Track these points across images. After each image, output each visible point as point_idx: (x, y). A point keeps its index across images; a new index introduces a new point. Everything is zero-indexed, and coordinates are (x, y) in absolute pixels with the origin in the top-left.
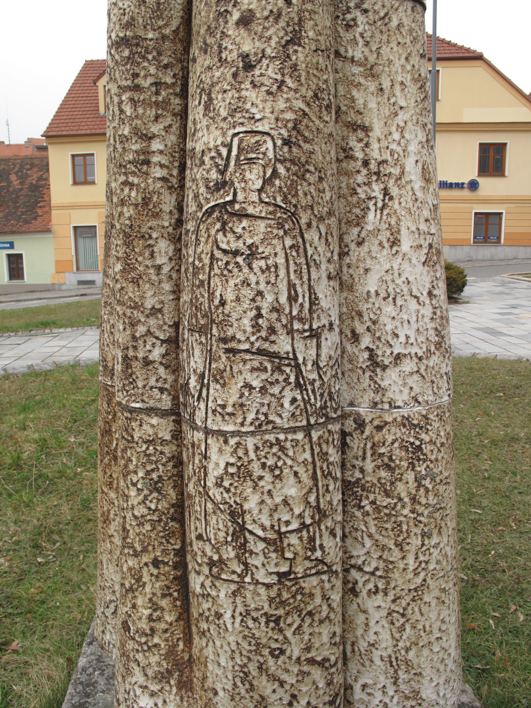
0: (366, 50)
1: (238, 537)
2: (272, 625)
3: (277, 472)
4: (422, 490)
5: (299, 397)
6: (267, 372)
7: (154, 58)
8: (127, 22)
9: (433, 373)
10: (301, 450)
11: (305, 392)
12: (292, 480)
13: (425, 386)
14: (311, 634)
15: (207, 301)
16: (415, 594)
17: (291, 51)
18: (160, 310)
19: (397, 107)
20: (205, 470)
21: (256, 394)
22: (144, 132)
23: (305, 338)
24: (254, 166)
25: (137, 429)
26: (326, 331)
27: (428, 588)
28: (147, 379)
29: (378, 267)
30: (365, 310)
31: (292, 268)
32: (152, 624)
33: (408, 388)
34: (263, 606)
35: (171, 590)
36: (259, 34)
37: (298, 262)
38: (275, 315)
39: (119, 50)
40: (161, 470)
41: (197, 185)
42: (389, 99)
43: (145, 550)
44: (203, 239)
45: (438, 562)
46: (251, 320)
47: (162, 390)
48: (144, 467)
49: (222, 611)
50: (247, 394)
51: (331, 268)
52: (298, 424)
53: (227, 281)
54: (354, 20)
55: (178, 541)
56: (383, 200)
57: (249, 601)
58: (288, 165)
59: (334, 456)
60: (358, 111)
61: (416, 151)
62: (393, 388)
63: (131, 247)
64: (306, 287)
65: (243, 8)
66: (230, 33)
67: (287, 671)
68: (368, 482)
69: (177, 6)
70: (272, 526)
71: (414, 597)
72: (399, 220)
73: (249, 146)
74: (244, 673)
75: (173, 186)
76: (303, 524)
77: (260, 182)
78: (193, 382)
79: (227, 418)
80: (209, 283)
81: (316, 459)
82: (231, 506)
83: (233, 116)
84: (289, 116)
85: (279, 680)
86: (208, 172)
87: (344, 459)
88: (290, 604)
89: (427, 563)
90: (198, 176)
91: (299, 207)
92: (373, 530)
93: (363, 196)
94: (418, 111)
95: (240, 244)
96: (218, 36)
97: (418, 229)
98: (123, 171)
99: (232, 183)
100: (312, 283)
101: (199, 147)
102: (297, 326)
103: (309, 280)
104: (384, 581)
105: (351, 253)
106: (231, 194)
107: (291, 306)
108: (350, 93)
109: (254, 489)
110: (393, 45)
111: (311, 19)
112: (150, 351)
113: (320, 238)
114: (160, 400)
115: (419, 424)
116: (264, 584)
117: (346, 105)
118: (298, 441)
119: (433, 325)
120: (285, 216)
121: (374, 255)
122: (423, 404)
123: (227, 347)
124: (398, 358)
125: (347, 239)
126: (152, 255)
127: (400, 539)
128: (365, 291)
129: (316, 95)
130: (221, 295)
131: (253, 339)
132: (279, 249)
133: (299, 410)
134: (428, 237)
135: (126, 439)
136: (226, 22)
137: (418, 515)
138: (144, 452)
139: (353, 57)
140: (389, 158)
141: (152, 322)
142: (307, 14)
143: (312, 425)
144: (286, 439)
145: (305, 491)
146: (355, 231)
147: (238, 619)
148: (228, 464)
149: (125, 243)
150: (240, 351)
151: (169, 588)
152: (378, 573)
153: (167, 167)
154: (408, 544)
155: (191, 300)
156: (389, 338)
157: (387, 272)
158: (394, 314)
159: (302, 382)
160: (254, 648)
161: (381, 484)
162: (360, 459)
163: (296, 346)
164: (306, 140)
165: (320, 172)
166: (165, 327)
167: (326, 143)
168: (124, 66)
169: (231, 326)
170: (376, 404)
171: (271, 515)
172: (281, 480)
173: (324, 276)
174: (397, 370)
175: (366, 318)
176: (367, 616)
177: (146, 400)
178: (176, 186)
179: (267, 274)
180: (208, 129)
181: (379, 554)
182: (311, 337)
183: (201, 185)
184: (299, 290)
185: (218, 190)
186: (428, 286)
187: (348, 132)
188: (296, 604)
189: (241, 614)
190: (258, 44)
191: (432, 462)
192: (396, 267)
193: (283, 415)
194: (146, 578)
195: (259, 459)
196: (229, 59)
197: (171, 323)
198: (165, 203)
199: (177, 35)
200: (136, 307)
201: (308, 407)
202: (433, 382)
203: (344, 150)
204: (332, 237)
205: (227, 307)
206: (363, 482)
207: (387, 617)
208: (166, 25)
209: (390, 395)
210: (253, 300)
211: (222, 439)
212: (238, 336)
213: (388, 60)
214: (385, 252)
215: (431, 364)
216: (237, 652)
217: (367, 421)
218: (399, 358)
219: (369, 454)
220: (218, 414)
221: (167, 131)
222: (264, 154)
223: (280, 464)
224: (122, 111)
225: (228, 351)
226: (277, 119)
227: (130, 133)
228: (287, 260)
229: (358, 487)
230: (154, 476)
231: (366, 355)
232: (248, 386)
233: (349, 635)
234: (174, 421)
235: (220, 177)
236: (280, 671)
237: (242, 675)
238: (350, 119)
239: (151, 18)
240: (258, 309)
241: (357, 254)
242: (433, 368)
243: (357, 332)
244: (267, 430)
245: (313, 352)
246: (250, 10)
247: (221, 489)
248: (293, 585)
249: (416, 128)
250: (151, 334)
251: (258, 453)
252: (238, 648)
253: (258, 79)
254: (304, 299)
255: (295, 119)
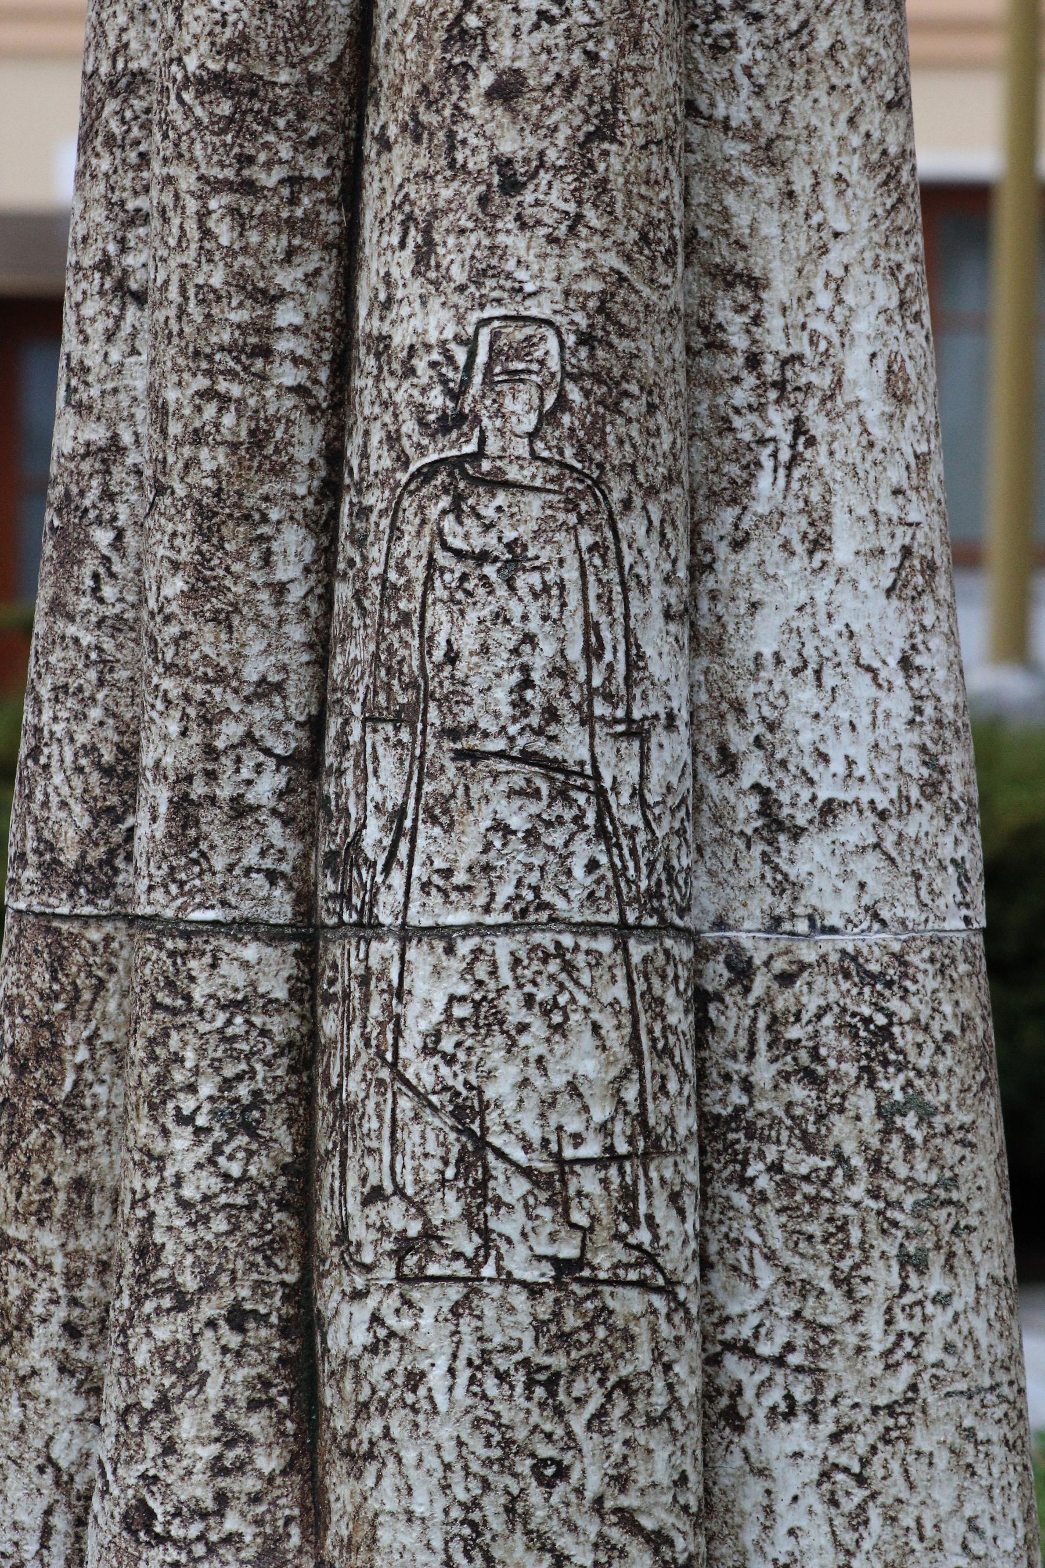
0: (757, 104)
1: (470, 1166)
2: (540, 1392)
3: (557, 1018)
4: (896, 1140)
5: (603, 859)
6: (540, 799)
7: (289, 125)
8: (230, 41)
9: (918, 853)
10: (607, 977)
11: (615, 851)
12: (587, 1040)
13: (897, 884)
14: (626, 1443)
15: (416, 655)
16: (890, 1422)
17: (596, 153)
18: (278, 687)
19: (826, 234)
20: (397, 1025)
21: (516, 843)
22: (261, 285)
23: (616, 736)
24: (522, 386)
25: (202, 977)
26: (659, 729)
27: (924, 1411)
28: (238, 849)
29: (779, 598)
30: (749, 697)
31: (593, 590)
32: (222, 1482)
33: (854, 883)
34: (520, 1341)
35: (273, 1391)
36: (533, 120)
37: (605, 578)
38: (557, 684)
39: (206, 98)
40: (259, 1077)
41: (396, 416)
42: (808, 217)
43: (209, 1285)
44: (409, 529)
45: (949, 1348)
46: (511, 692)
47: (272, 877)
48: (217, 1070)
49: (423, 1365)
50: (498, 844)
51: (673, 595)
52: (602, 918)
53: (462, 613)
54: (730, 35)
55: (294, 1264)
56: (793, 446)
57: (490, 1328)
58: (587, 384)
59: (679, 1017)
60: (737, 242)
61: (872, 332)
62: (818, 881)
63: (215, 540)
64: (619, 630)
65: (501, 66)
66: (474, 111)
67: (573, 1529)
68: (761, 1114)
69: (340, 10)
70: (545, 1142)
71: (888, 1429)
72: (829, 491)
73: (511, 347)
74: (473, 1525)
75: (318, 406)
76: (610, 1149)
77: (533, 418)
78: (374, 833)
79: (454, 896)
80: (422, 618)
81: (639, 1005)
82: (458, 1094)
83: (479, 285)
84: (591, 285)
85: (553, 1550)
86: (424, 391)
87: (704, 1060)
88: (580, 1346)
89: (918, 1340)
90: (399, 397)
91: (608, 467)
92: (777, 1240)
93: (747, 436)
94: (877, 237)
95: (491, 539)
96: (447, 112)
97: (874, 512)
98: (204, 365)
99: (477, 420)
100: (632, 623)
101: (401, 338)
102: (600, 708)
103: (627, 616)
104: (808, 1380)
105: (718, 566)
106: (475, 440)
107: (589, 668)
108: (718, 197)
109: (509, 1051)
110: (820, 92)
111: (637, 84)
112: (249, 783)
113: (648, 531)
114: (267, 901)
115: (883, 974)
116: (523, 1284)
117: (709, 227)
118: (601, 954)
119: (914, 737)
120: (580, 487)
121: (771, 571)
122: (894, 927)
123: (458, 746)
124: (829, 810)
125: (710, 533)
126: (267, 560)
127: (845, 1265)
128: (751, 654)
129: (644, 237)
130: (449, 642)
131: (513, 730)
132: (567, 551)
133: (602, 886)
134: (899, 531)
135: (166, 1008)
136: (466, 88)
137: (889, 1204)
138: (220, 1031)
139: (727, 118)
140: (808, 351)
141: (258, 712)
142: (628, 75)
143: (630, 928)
144: (577, 948)
145: (614, 1072)
146: (729, 514)
147: (464, 1375)
148: (452, 998)
149: (199, 530)
150: (487, 755)
151: (267, 1384)
152: (794, 1359)
153: (308, 363)
154: (866, 1280)
155: (376, 656)
156: (807, 763)
157: (800, 609)
158: (817, 707)
159: (610, 828)
160: (497, 1453)
161: (793, 1118)
162: (742, 1057)
163: (598, 750)
164: (624, 332)
165: (650, 393)
166: (289, 727)
167: (663, 332)
168: (218, 134)
169: (469, 703)
170: (777, 921)
171: (542, 1116)
172: (564, 1036)
173: (657, 610)
174: (827, 838)
175: (753, 716)
176: (769, 1484)
177: (233, 901)
178: (324, 405)
179: (543, 600)
180: (424, 303)
181: (795, 1305)
182: (628, 735)
183: (405, 415)
184: (606, 634)
185: (446, 430)
186: (900, 644)
187: (715, 289)
188: (595, 1348)
189: (470, 1363)
190: (530, 140)
191: (919, 1074)
192: (821, 598)
193: (572, 894)
194: (209, 1359)
195: (520, 986)
196: (471, 166)
197: (302, 719)
198: (301, 444)
199: (338, 73)
200: (221, 678)
201: (623, 884)
202: (917, 876)
203: (705, 330)
204: (675, 528)
205: (462, 666)
206: (750, 1114)
207: (819, 1484)
208: (317, 53)
209: (810, 897)
210: (516, 651)
211: (440, 946)
212: (482, 725)
213: (807, 127)
214: (796, 564)
215: (911, 831)
216: (458, 1467)
217: (757, 961)
218: (831, 811)
219: (762, 1045)
220: (434, 891)
221: (310, 284)
222: (542, 363)
223: (562, 1000)
224: (206, 233)
225: (460, 755)
226: (567, 293)
227: (227, 283)
228: (583, 575)
229: (737, 1131)
230: (243, 1090)
231: (753, 802)
232: (501, 827)
233: (724, 1550)
234: (296, 954)
235: (450, 405)
236: (555, 1524)
237: (466, 1531)
238: (718, 260)
239: (285, 40)
240: (525, 669)
241: (732, 567)
242: (917, 841)
243: (733, 749)
244: (537, 923)
245: (633, 767)
246: (517, 72)
247: (437, 1060)
248: (588, 1297)
249: (871, 279)
250: (255, 741)
251: (519, 971)
252: (460, 1456)
253: (529, 211)
254: (615, 655)
255: (603, 292)
